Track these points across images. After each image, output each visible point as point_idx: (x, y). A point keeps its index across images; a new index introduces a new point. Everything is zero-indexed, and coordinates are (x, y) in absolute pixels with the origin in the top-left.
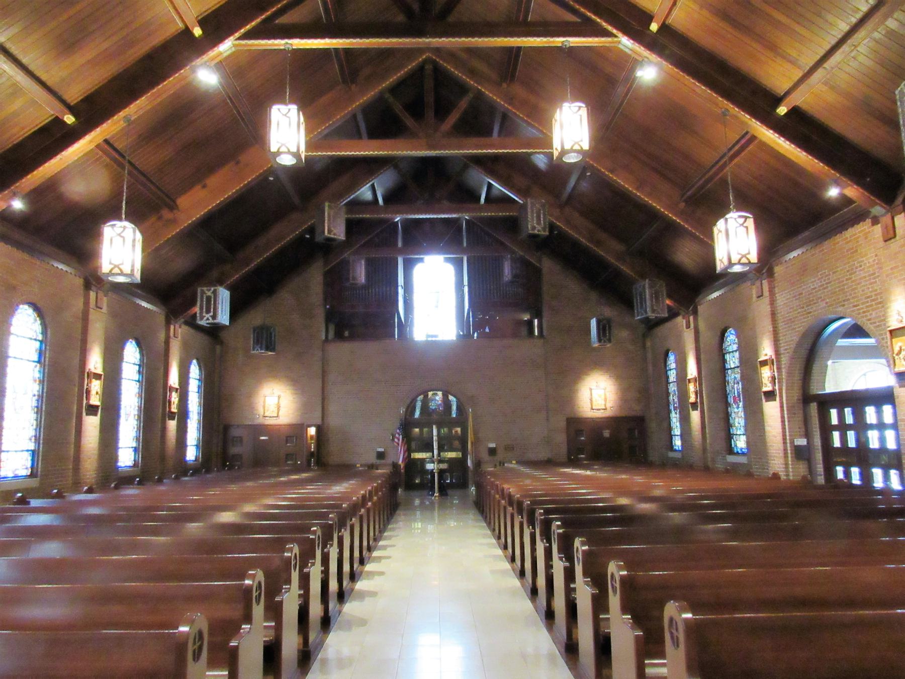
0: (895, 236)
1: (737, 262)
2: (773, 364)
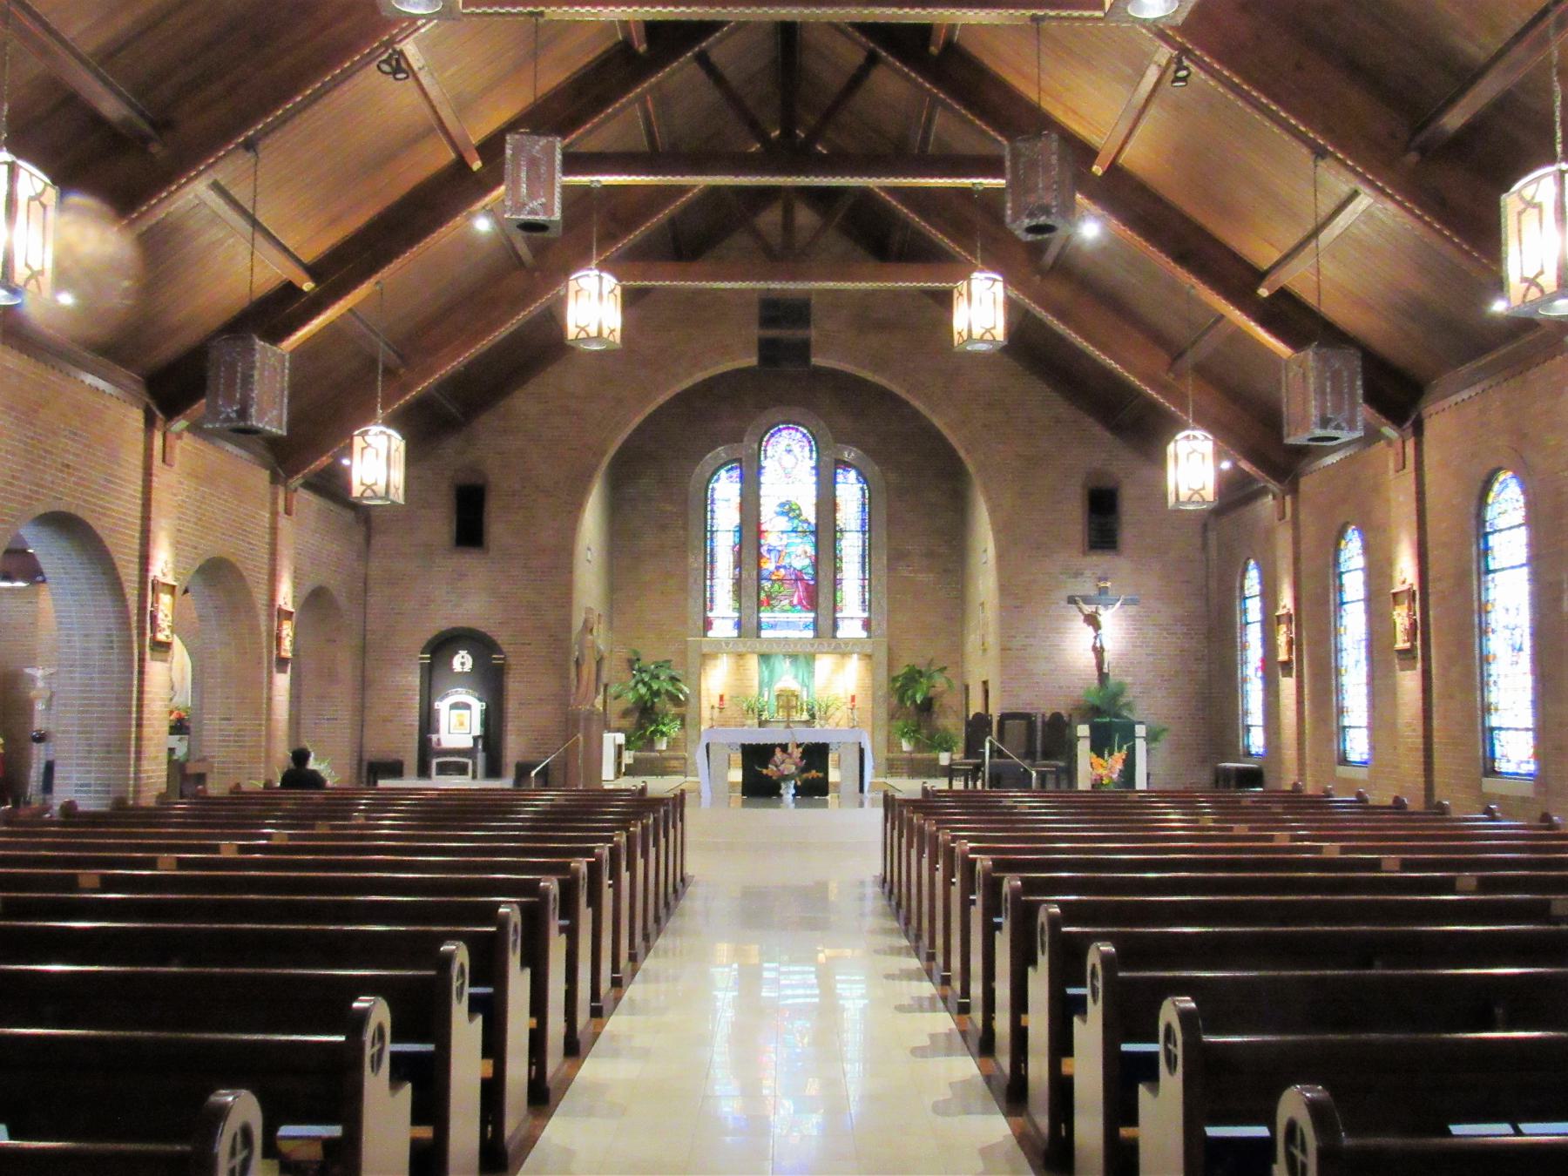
0: (1404, 467)
1: (1185, 500)
2: (1414, 600)
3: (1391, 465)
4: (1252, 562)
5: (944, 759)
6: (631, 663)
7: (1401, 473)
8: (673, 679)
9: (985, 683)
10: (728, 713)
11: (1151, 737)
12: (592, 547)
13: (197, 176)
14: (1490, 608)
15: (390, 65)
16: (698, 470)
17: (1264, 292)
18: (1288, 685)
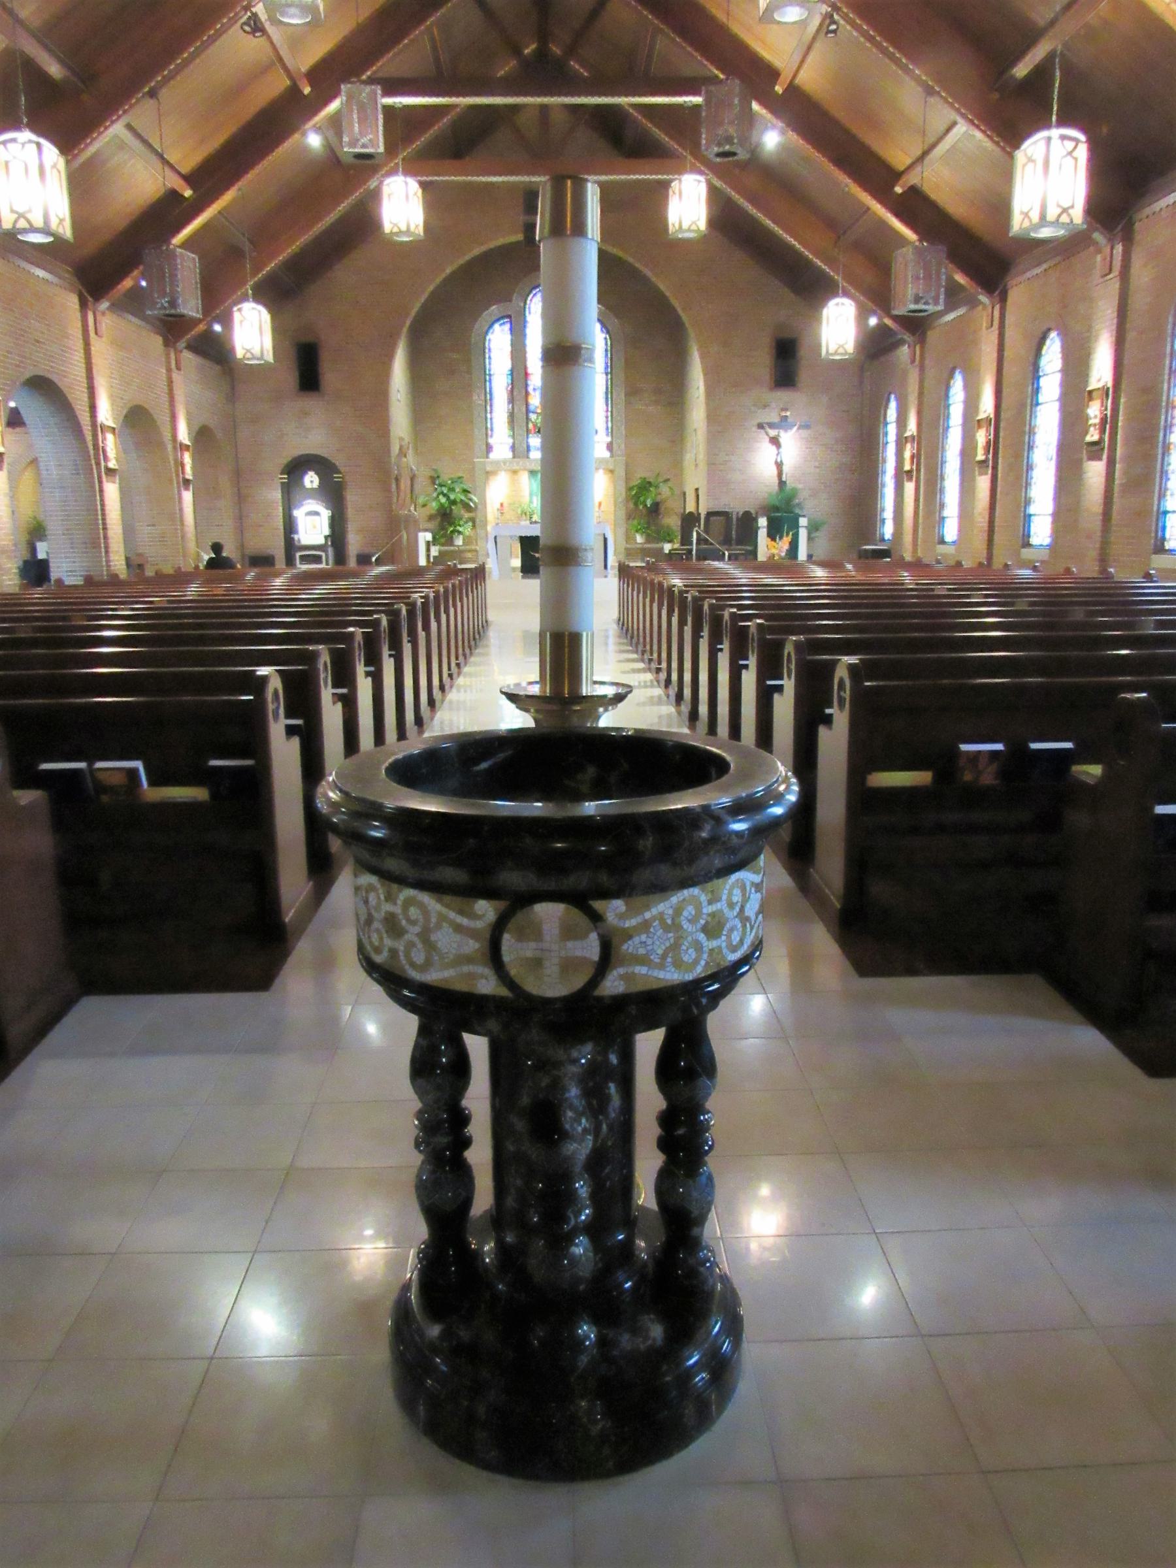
2: (990, 424)
3: (984, 325)
4: (893, 396)
5: (667, 547)
6: (433, 480)
7: (990, 330)
8: (466, 491)
9: (697, 490)
10: (507, 516)
11: (813, 528)
12: (400, 390)
13: (117, 120)
14: (1036, 430)
15: (249, 25)
16: (477, 326)
17: (898, 190)
18: (909, 487)
